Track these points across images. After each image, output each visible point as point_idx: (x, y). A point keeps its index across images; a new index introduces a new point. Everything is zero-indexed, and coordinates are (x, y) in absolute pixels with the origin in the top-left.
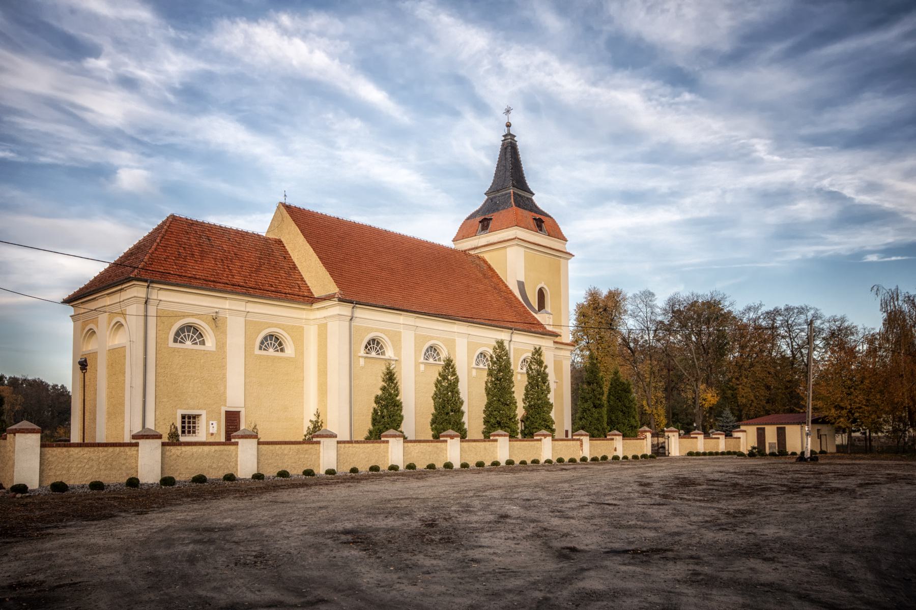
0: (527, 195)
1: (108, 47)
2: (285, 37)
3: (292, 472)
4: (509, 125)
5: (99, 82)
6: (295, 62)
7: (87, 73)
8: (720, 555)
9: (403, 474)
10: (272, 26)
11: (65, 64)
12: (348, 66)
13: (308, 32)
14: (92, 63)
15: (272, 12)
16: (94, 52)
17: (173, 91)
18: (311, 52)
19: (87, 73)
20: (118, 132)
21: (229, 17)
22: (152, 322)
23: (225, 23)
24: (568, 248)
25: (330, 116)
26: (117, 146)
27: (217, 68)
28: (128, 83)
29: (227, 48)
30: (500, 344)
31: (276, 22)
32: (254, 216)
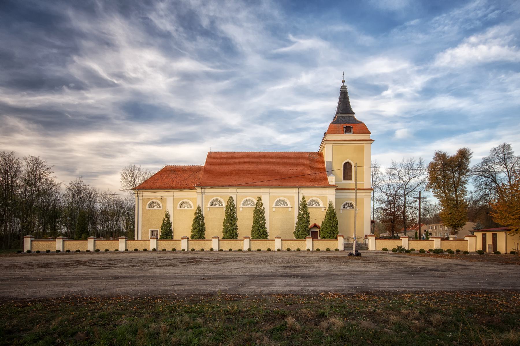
0: (351, 115)
1: (391, 85)
2: (474, 48)
3: (331, 249)
4: (344, 82)
5: (388, 99)
6: (479, 58)
7: (383, 98)
8: (188, 312)
9: (417, 254)
10: (465, 45)
11: (375, 97)
12: (514, 47)
13: (486, 40)
14: (385, 93)
15: (465, 39)
16: (386, 88)
17: (418, 92)
18: (489, 48)
19: (383, 98)
20: (396, 116)
21: (442, 51)
22: (140, 201)
23: (441, 54)
24: (371, 137)
25: (503, 76)
26: (396, 122)
27: (438, 75)
28: (399, 96)
29: (442, 65)
30: (231, 198)
31: (468, 42)
32: (460, 136)
